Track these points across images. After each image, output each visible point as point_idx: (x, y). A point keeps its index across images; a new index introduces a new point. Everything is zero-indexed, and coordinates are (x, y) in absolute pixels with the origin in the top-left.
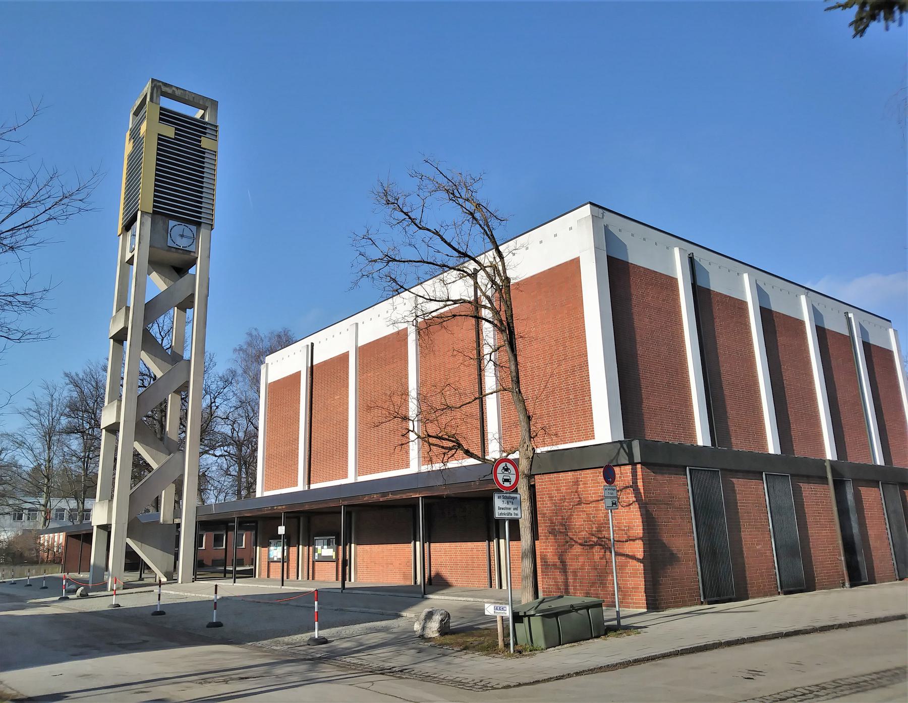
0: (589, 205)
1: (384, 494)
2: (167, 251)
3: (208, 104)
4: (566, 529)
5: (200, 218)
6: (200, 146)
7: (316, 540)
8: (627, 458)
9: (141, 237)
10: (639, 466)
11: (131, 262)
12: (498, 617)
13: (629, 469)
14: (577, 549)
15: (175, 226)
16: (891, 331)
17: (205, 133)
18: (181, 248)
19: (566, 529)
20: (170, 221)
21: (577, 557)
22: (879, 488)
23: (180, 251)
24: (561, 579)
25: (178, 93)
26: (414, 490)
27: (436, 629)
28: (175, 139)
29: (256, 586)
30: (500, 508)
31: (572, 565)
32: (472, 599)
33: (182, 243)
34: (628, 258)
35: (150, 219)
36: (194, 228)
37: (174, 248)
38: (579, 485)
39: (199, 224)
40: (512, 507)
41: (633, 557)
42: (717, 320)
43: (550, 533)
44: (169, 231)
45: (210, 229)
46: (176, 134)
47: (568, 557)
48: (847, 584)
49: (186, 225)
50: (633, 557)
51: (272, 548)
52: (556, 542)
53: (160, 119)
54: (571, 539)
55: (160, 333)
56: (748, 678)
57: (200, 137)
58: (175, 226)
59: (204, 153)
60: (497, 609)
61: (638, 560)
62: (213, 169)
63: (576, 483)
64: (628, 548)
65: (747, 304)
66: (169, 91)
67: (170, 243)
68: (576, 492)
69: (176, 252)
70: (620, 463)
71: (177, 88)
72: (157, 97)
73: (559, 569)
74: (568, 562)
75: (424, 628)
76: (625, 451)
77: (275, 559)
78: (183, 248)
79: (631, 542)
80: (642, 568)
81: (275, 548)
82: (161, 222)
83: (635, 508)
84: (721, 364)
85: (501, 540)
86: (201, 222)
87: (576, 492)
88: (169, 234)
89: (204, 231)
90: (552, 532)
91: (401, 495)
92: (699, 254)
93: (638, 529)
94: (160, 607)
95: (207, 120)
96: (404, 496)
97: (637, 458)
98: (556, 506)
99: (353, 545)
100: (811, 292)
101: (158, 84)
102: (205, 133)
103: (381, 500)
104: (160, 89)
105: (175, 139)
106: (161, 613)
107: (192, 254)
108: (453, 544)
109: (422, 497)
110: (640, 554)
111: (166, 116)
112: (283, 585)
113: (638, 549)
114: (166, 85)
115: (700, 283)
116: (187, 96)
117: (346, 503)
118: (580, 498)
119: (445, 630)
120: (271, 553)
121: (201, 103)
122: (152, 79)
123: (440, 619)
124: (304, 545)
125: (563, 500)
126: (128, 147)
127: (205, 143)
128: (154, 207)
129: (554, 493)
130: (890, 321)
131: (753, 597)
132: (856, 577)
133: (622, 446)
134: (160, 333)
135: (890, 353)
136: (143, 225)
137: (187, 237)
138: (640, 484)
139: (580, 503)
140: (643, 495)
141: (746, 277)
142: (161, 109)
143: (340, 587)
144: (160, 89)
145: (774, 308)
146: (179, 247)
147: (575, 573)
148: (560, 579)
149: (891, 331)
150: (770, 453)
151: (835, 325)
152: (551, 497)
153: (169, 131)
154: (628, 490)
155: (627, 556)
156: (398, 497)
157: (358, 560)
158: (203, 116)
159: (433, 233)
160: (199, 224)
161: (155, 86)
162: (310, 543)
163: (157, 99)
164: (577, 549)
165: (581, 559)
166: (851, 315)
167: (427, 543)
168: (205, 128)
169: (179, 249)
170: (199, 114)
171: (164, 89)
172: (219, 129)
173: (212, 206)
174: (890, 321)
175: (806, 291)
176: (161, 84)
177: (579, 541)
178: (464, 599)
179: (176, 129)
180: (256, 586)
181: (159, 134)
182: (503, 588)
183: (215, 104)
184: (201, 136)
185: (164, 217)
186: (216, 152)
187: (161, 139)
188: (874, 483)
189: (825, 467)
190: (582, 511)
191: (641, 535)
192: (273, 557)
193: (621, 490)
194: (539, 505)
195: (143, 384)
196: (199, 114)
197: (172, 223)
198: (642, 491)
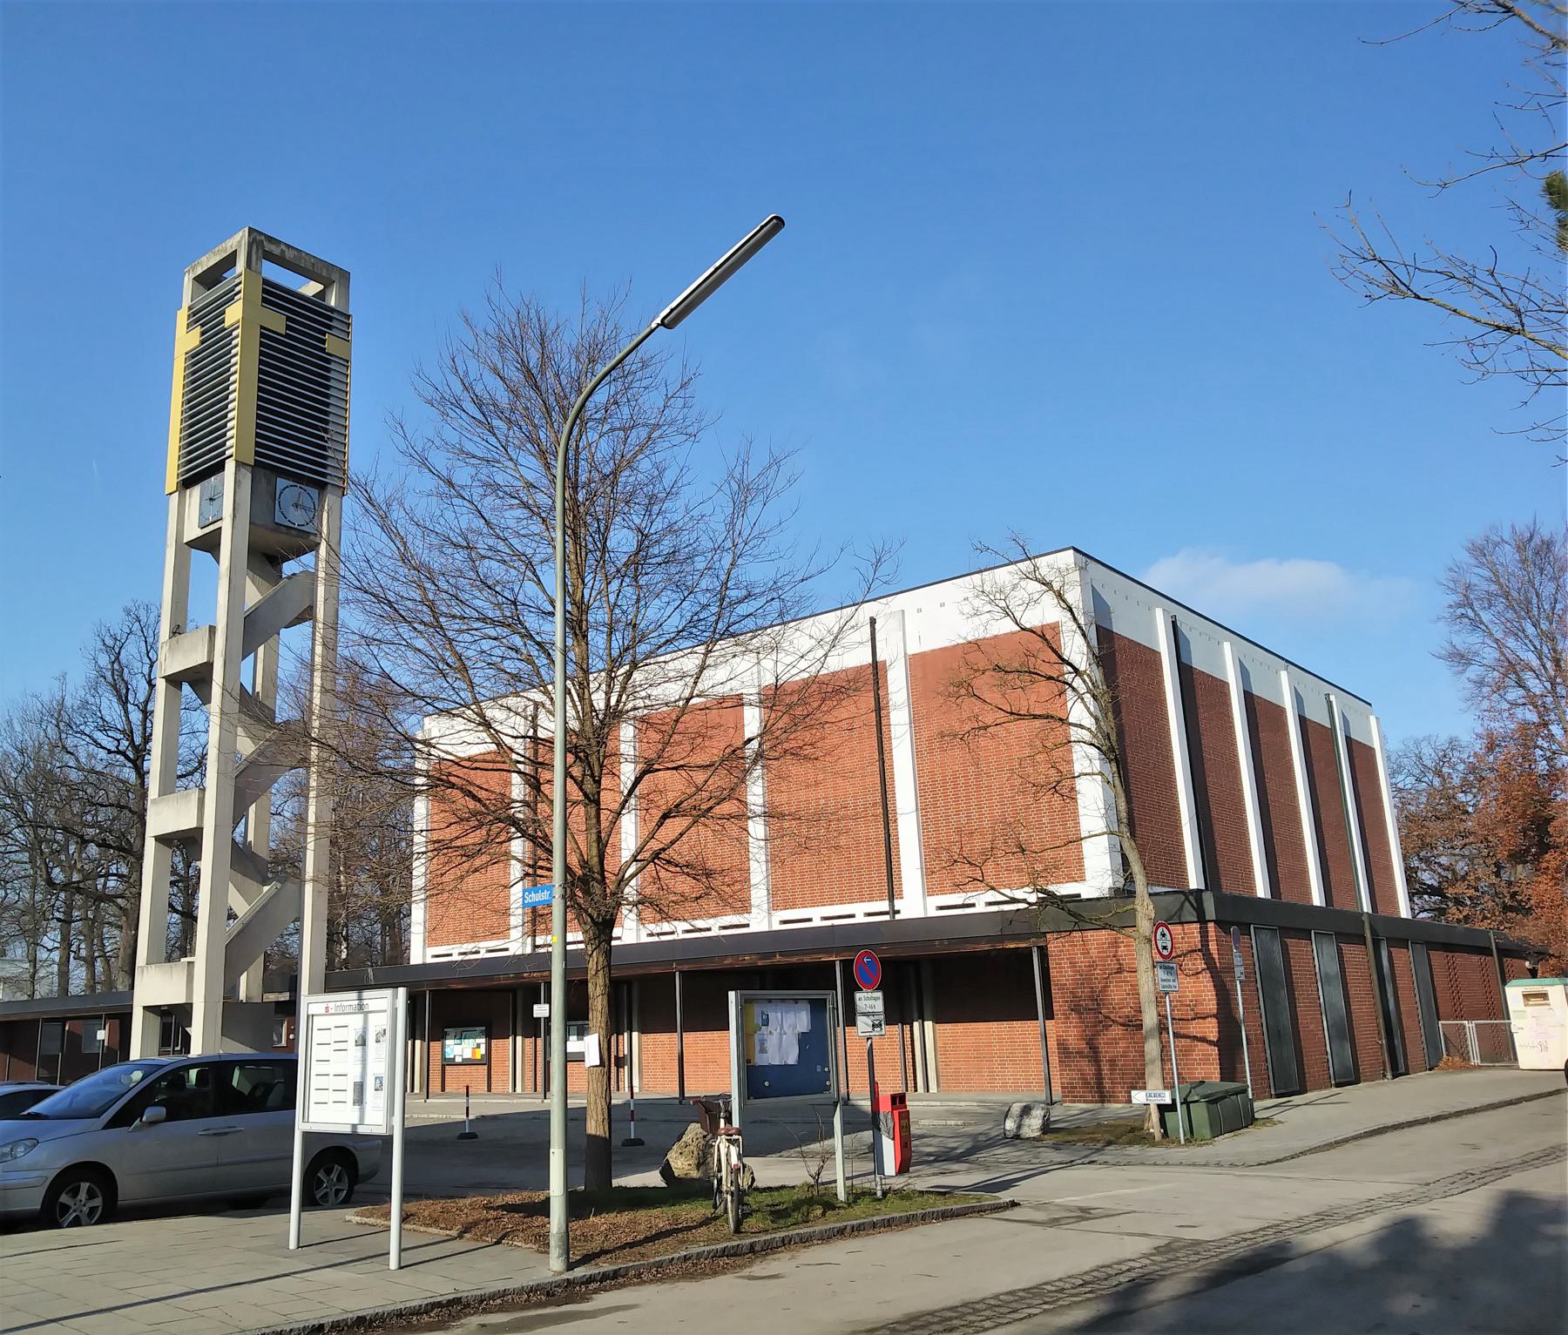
0: (1072, 550)
1: (765, 956)
2: (273, 530)
3: (335, 277)
4: (1098, 1004)
5: (324, 475)
6: (323, 350)
7: (569, 1026)
8: (1195, 913)
9: (236, 506)
10: (1211, 925)
11: (209, 543)
12: (1152, 1106)
13: (1196, 928)
14: (1116, 1031)
15: (287, 487)
16: (1373, 719)
17: (330, 327)
18: (296, 526)
19: (1098, 1004)
20: (278, 479)
21: (1113, 1042)
22: (1311, 940)
23: (293, 532)
24: (1090, 1070)
25: (289, 255)
26: (828, 951)
27: (1039, 1126)
28: (287, 336)
29: (484, 1101)
30: (1163, 980)
31: (1106, 1052)
32: (938, 1103)
33: (297, 518)
34: (1112, 627)
35: (250, 475)
36: (314, 492)
37: (285, 526)
38: (1120, 947)
39: (322, 486)
40: (1169, 977)
41: (1203, 1040)
42: (1201, 710)
43: (1072, 1010)
44: (277, 498)
45: (341, 493)
46: (288, 327)
47: (1102, 1041)
48: (1389, 1075)
49: (303, 486)
50: (1203, 1040)
51: (448, 1042)
52: (1083, 1022)
53: (264, 300)
54: (1106, 1017)
55: (148, 653)
56: (1180, 1226)
57: (324, 334)
58: (287, 487)
59: (328, 361)
60: (1150, 1096)
61: (1211, 1043)
62: (343, 391)
63: (1115, 944)
64: (1195, 1028)
65: (1229, 686)
66: (276, 250)
67: (279, 519)
68: (1114, 956)
69: (287, 534)
70: (1183, 920)
71: (288, 246)
72: (257, 259)
73: (1087, 1057)
74: (1103, 1048)
75: (1019, 1127)
76: (1192, 905)
77: (458, 1060)
78: (299, 528)
79: (1201, 1021)
80: (1217, 1052)
81: (459, 1041)
82: (263, 481)
83: (1206, 978)
84: (1207, 773)
85: (926, 1023)
86: (327, 483)
87: (1114, 956)
88: (277, 502)
89: (330, 499)
90: (1076, 1009)
91: (802, 958)
92: (1185, 621)
93: (1211, 1005)
94: (470, 1125)
95: (333, 303)
96: (807, 959)
97: (1210, 912)
98: (1081, 975)
99: (635, 1035)
100: (1291, 666)
101: (259, 238)
102: (330, 327)
103: (759, 964)
104: (263, 246)
105: (287, 336)
106: (472, 1136)
107: (312, 537)
108: (960, 1027)
109: (840, 961)
110: (1214, 1036)
111: (273, 295)
112: (545, 1098)
113: (1211, 1029)
114: (271, 239)
115: (1184, 660)
116: (303, 261)
117: (686, 968)
118: (1120, 964)
119: (1046, 1128)
120: (447, 1050)
121: (324, 274)
122: (250, 228)
123: (1042, 1114)
124: (525, 1036)
125: (1092, 966)
126: (187, 339)
127: (332, 344)
128: (257, 453)
129: (1080, 958)
130: (1370, 704)
131: (1311, 1090)
132: (1398, 1068)
133: (1187, 899)
134: (148, 653)
135: (1371, 750)
136: (239, 486)
137: (304, 508)
138: (1213, 947)
139: (1120, 971)
140: (1217, 961)
141: (1227, 646)
142: (266, 282)
143: (678, 1096)
144: (263, 246)
145: (1255, 692)
146: (293, 526)
147: (1112, 1062)
148: (1089, 1070)
149: (1373, 719)
150: (1315, 904)
151: (1317, 715)
152: (1073, 964)
153: (277, 322)
154: (1195, 955)
155: (1195, 1038)
156: (794, 959)
157: (644, 1057)
158: (321, 295)
159: (1039, 636)
160: (322, 486)
161: (254, 239)
162: (440, 1036)
163: (257, 264)
164: (1116, 1031)
165: (1122, 1044)
166: (1332, 698)
167: (900, 1024)
168: (331, 318)
169: (291, 528)
170: (311, 288)
171: (268, 247)
172: (354, 321)
173: (342, 455)
174: (1370, 704)
175: (1286, 664)
176: (263, 238)
177: (1121, 1020)
178: (924, 1103)
179: (288, 319)
180: (484, 1101)
181: (262, 327)
182: (931, 1091)
183: (345, 276)
184: (326, 332)
185: (268, 472)
186: (348, 362)
187: (266, 335)
188: (1402, 943)
189: (1363, 922)
190: (1124, 982)
191: (1215, 1011)
192: (452, 1056)
193: (1185, 955)
194: (1053, 973)
195: (117, 748)
196: (311, 288)
197: (281, 483)
198: (1216, 956)
